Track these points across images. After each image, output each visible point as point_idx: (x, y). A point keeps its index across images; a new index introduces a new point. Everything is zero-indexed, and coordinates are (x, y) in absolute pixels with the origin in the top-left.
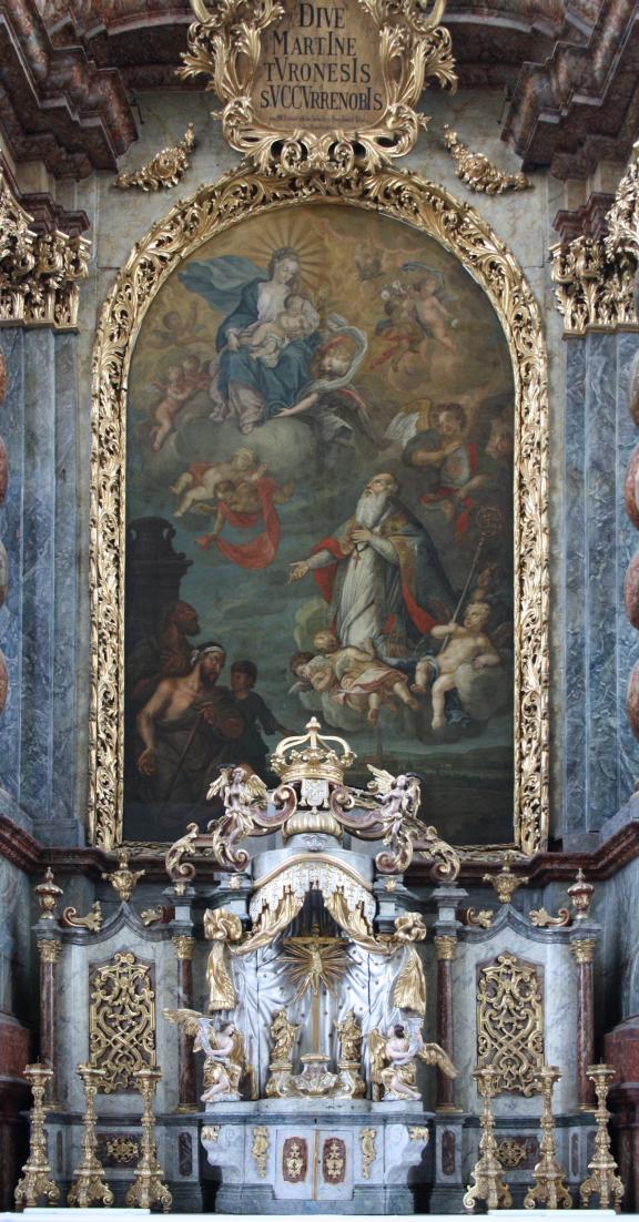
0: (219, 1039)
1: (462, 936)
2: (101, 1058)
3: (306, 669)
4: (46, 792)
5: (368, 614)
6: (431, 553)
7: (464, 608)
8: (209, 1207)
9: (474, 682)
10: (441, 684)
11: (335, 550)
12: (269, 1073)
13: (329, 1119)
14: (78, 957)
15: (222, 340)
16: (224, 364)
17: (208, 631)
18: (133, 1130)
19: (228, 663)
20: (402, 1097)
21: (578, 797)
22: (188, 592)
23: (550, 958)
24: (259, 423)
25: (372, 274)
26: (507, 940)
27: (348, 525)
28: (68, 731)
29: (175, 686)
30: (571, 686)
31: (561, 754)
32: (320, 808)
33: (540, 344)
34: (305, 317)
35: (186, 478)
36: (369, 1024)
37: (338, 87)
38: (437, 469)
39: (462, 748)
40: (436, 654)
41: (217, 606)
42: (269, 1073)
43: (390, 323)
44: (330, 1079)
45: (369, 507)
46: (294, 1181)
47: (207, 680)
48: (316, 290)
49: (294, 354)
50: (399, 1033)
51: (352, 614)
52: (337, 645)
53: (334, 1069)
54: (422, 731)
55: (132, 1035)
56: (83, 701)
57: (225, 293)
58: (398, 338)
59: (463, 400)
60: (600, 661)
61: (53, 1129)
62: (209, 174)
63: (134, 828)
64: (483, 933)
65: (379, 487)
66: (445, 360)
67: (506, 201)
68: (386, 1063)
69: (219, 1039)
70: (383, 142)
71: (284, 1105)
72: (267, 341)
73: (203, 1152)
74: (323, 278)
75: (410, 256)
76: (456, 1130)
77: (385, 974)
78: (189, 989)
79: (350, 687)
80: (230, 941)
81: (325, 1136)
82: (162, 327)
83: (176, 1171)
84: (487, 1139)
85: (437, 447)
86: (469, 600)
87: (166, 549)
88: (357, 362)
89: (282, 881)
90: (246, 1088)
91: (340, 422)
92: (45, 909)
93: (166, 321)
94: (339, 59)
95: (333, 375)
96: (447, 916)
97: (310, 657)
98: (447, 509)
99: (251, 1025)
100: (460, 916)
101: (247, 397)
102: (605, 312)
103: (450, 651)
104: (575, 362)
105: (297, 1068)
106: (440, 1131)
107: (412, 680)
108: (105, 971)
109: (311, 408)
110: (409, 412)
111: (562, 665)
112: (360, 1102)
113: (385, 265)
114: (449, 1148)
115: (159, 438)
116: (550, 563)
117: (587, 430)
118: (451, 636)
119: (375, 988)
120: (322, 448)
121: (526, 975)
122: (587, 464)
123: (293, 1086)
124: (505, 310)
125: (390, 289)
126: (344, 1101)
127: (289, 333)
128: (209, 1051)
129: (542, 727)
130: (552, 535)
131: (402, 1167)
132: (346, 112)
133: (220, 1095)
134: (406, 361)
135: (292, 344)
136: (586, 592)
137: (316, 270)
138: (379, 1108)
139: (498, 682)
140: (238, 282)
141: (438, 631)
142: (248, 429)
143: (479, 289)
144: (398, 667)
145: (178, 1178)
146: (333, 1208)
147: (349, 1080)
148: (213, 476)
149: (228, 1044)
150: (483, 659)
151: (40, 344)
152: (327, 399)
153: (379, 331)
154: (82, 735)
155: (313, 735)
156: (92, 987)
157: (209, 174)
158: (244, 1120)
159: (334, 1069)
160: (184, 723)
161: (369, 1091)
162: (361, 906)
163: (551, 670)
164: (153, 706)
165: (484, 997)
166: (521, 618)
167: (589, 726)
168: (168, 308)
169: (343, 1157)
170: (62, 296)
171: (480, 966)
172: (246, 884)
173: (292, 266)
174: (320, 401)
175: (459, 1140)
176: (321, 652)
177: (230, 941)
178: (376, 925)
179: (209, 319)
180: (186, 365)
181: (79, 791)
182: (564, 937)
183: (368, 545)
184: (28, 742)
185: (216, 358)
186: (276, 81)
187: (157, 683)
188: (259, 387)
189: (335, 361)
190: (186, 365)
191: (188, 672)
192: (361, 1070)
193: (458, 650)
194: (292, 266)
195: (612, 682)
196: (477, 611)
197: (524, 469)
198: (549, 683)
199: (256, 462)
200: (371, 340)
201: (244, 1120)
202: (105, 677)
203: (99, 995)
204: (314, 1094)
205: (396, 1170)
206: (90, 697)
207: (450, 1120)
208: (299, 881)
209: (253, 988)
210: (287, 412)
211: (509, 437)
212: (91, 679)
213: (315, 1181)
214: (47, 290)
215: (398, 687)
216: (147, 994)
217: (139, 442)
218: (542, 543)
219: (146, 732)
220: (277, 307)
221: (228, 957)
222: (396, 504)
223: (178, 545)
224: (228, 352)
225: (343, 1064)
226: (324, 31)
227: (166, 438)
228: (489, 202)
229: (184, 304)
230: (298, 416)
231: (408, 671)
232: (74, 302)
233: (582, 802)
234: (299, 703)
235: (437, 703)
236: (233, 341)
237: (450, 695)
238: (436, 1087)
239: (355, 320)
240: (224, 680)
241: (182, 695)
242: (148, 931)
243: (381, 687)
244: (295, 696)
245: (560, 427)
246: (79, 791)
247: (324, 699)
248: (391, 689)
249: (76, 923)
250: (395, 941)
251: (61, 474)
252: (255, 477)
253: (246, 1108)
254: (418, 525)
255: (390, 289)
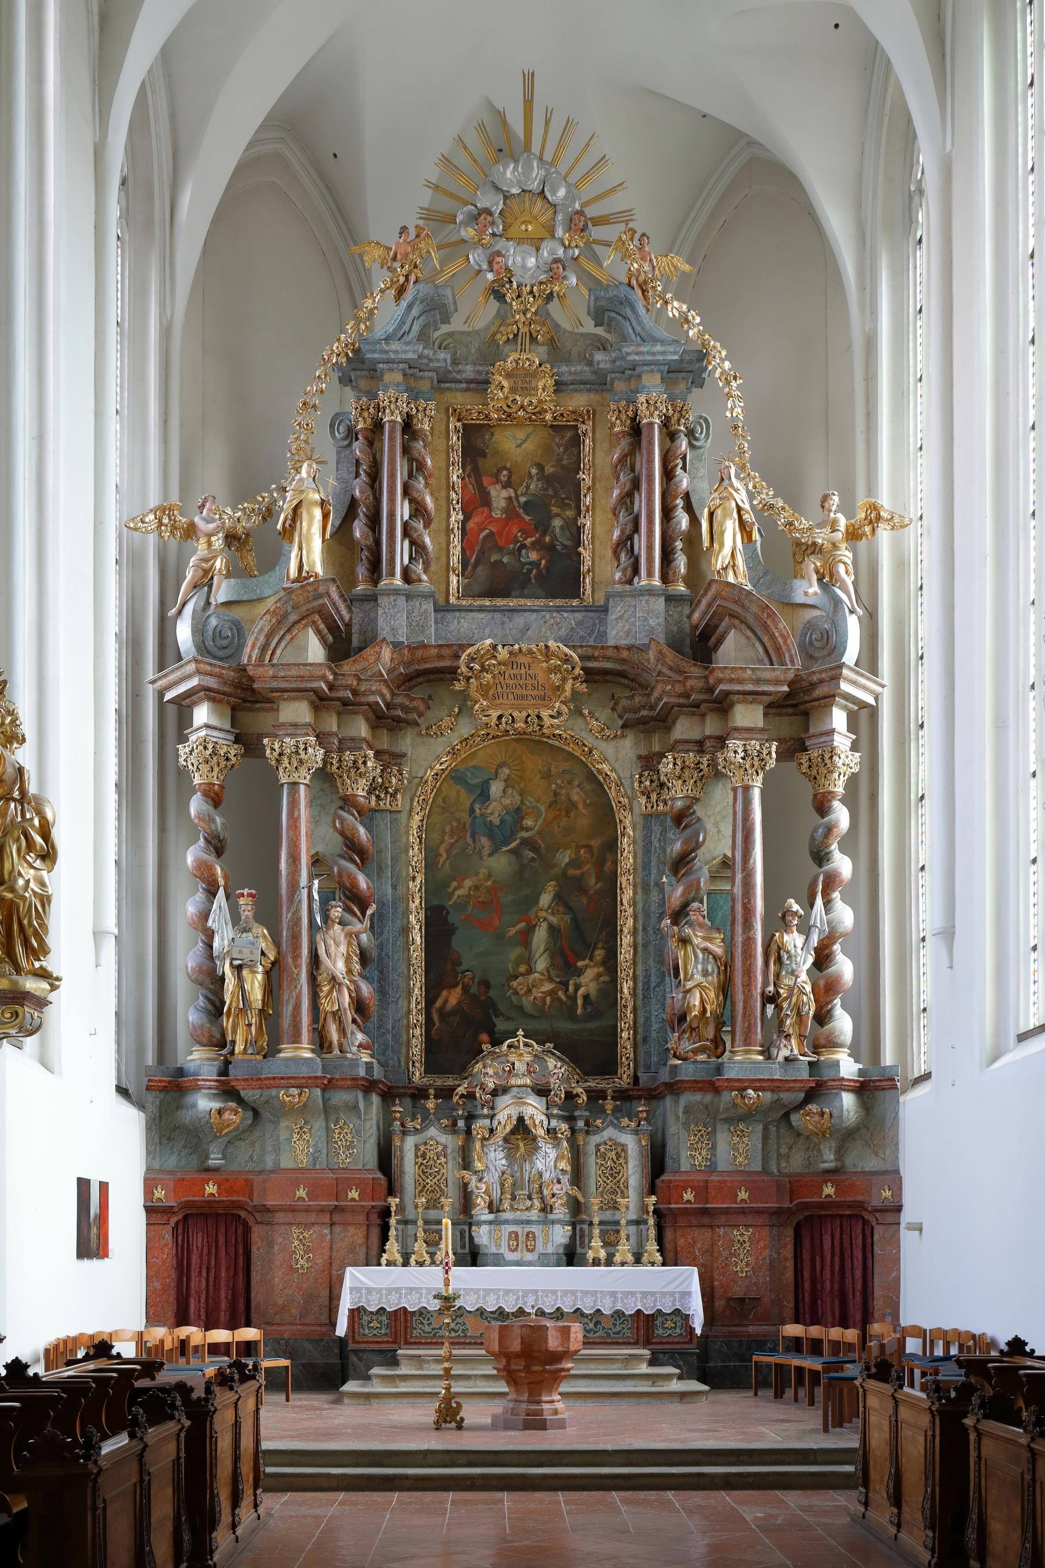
0: (479, 1185)
1: (587, 1133)
2: (421, 1191)
3: (514, 984)
4: (389, 1052)
5: (545, 955)
6: (576, 923)
7: (593, 952)
8: (474, 1264)
9: (598, 991)
10: (582, 991)
11: (528, 921)
12: (501, 1200)
13: (528, 1222)
14: (410, 1142)
15: (472, 811)
16: (473, 824)
17: (466, 965)
18: (435, 1227)
19: (476, 981)
20: (561, 1212)
21: (648, 1054)
22: (456, 943)
23: (629, 1140)
24: (490, 855)
25: (547, 776)
26: (609, 1133)
27: (535, 909)
28: (399, 1020)
29: (450, 993)
30: (644, 997)
31: (640, 1030)
32: (523, 1075)
33: (630, 817)
34: (513, 799)
35: (455, 884)
36: (546, 1176)
37: (530, 692)
38: (579, 880)
39: (592, 1025)
40: (579, 976)
41: (470, 950)
42: (501, 1200)
43: (556, 802)
44: (528, 1203)
45: (545, 899)
46: (513, 1251)
47: (466, 989)
48: (519, 784)
49: (508, 818)
50: (559, 1182)
51: (537, 955)
52: (530, 971)
53: (530, 1198)
54: (572, 1016)
55: (435, 1180)
56: (406, 1004)
57: (473, 786)
58: (560, 810)
59: (592, 843)
60: (658, 985)
61: (400, 1227)
62: (465, 729)
63: (431, 1068)
64: (599, 1130)
65: (550, 889)
66: (583, 820)
67: (613, 743)
68: (553, 1195)
69: (479, 1185)
70: (551, 716)
71: (508, 1215)
72: (495, 811)
73: (471, 1238)
74: (522, 778)
75: (566, 765)
76: (585, 1227)
77: (552, 1154)
78: (463, 1160)
79: (537, 993)
80: (484, 1139)
81: (527, 1230)
82: (441, 806)
83: (458, 1247)
84: (596, 1231)
85: (579, 867)
86: (595, 948)
87: (445, 921)
88: (540, 822)
89: (507, 1112)
90: (491, 1208)
91: (531, 854)
92: (395, 1119)
93: (444, 800)
94: (529, 682)
95: (527, 829)
96: (581, 1124)
97: (516, 977)
98: (584, 900)
99: (492, 1178)
100: (587, 1124)
101: (484, 841)
102: (661, 805)
103: (586, 974)
104: (647, 828)
105: (514, 1198)
106: (578, 1227)
107: (567, 990)
108: (422, 1148)
109: (517, 847)
110: (566, 849)
111: (640, 985)
112: (542, 1214)
113: (553, 771)
114: (582, 1236)
115: (441, 863)
116: (634, 932)
117: (653, 864)
118: (586, 966)
119: (548, 1160)
120: (522, 868)
121: (619, 1150)
122: (652, 884)
123: (512, 1206)
124: (612, 794)
125: (556, 783)
126: (534, 1214)
127: (505, 807)
128: (475, 1190)
129: (630, 1016)
130: (635, 917)
131: (561, 1245)
132: (533, 702)
133: (481, 1213)
134: (564, 822)
135: (507, 813)
136: (651, 948)
137: (519, 773)
138: (551, 1217)
139: (610, 989)
140: (480, 780)
141: (580, 964)
142: (485, 858)
143: (601, 785)
144: (560, 983)
145: (459, 1251)
146: (530, 1264)
147: (537, 1203)
148: (468, 883)
149: (484, 1187)
150: (602, 979)
151: (383, 819)
152: (525, 842)
153: (550, 806)
154: (405, 1021)
155: (522, 1039)
156: (416, 1156)
157: (465, 729)
158: (490, 1223)
159: (530, 1198)
160: (454, 1012)
161: (546, 1209)
162: (542, 1122)
163: (635, 989)
164: (438, 1003)
165: (599, 1161)
166: (621, 958)
167: (653, 1018)
168: (444, 794)
169: (534, 1240)
170: (393, 796)
171: (598, 1146)
172: (491, 1112)
173: (506, 771)
174: (521, 843)
175: (587, 1232)
176: (522, 975)
177: (484, 1139)
178: (548, 1130)
179: (466, 799)
180: (454, 824)
181: (404, 1051)
182: (636, 1132)
183: (545, 919)
184: (379, 1027)
185: (469, 820)
186: (499, 689)
187: (441, 991)
188: (491, 836)
189: (528, 822)
190: (454, 824)
191: (455, 986)
192: (542, 1199)
193: (590, 974)
194: (506, 771)
195: (664, 996)
196: (599, 954)
197: (623, 880)
198: (634, 994)
199: (489, 876)
200: (546, 811)
201: (490, 1223)
202: (416, 991)
203: (420, 1160)
204: (521, 1210)
205: (559, 1246)
206: (409, 1002)
207: (583, 1222)
208: (514, 1112)
209: (493, 1159)
210: (505, 849)
211: (615, 862)
212: (409, 993)
213: (522, 1251)
214: (387, 792)
215: (560, 993)
216: (443, 1160)
217: (430, 865)
218: (630, 922)
219: (435, 1017)
220: (500, 793)
221: (483, 1146)
222: (558, 897)
223: (451, 919)
224: (475, 817)
225: (534, 1196)
226: (523, 671)
227: (444, 862)
228: (605, 743)
229: (453, 791)
230: (510, 851)
231: (565, 984)
232: (399, 796)
233: (650, 1057)
234: (511, 1001)
235: (580, 1002)
236: (478, 811)
237: (586, 997)
238: (576, 1207)
239: (538, 801)
240: (474, 990)
241: (452, 998)
242: (445, 1130)
243: (552, 993)
244: (510, 997)
245: (639, 861)
246: (404, 1051)
247: (524, 999)
248: (557, 994)
249: (410, 1125)
250: (556, 1138)
251: (394, 887)
252: (489, 883)
253: (491, 1217)
254: (570, 909)
255: (556, 783)
